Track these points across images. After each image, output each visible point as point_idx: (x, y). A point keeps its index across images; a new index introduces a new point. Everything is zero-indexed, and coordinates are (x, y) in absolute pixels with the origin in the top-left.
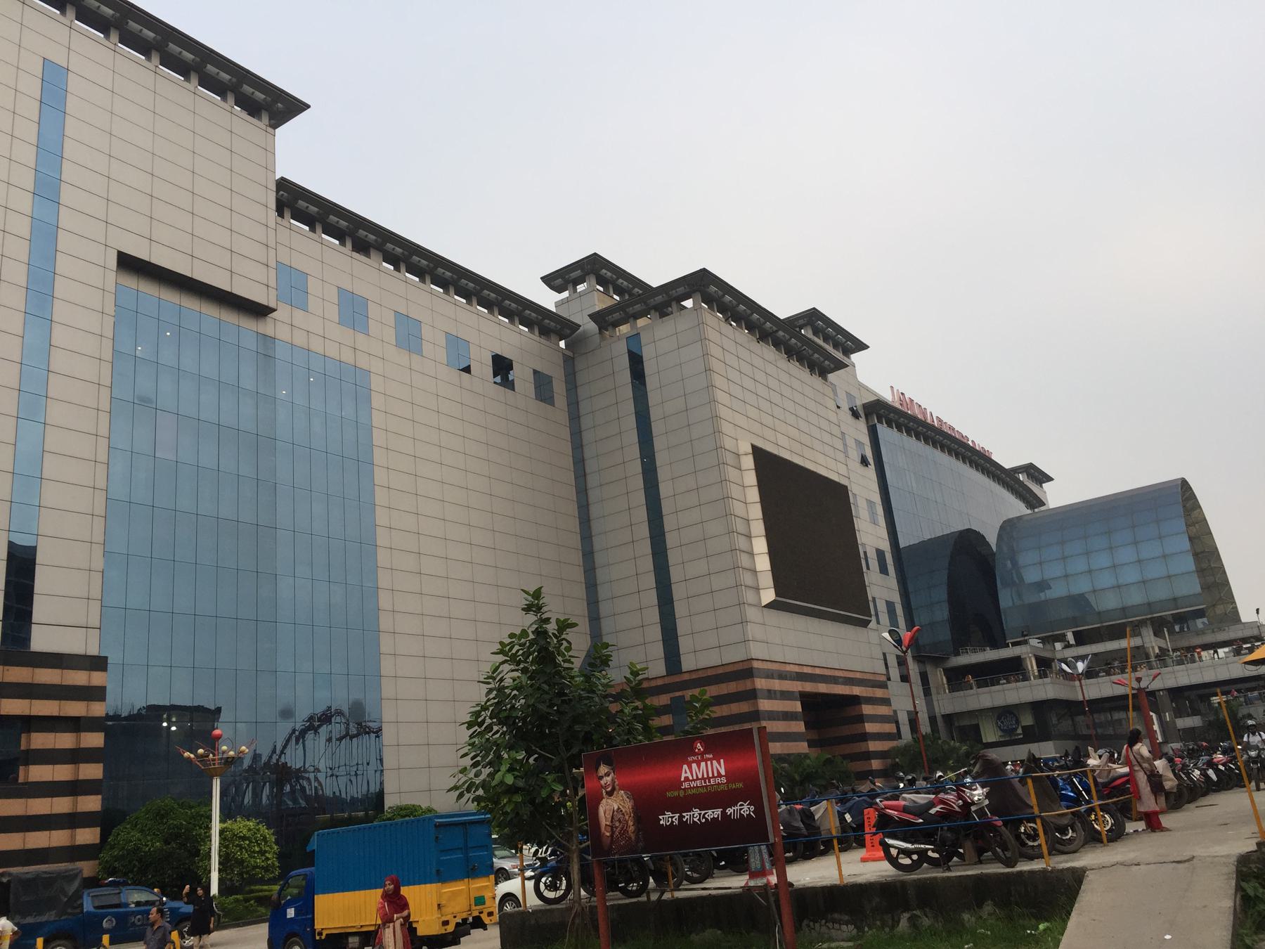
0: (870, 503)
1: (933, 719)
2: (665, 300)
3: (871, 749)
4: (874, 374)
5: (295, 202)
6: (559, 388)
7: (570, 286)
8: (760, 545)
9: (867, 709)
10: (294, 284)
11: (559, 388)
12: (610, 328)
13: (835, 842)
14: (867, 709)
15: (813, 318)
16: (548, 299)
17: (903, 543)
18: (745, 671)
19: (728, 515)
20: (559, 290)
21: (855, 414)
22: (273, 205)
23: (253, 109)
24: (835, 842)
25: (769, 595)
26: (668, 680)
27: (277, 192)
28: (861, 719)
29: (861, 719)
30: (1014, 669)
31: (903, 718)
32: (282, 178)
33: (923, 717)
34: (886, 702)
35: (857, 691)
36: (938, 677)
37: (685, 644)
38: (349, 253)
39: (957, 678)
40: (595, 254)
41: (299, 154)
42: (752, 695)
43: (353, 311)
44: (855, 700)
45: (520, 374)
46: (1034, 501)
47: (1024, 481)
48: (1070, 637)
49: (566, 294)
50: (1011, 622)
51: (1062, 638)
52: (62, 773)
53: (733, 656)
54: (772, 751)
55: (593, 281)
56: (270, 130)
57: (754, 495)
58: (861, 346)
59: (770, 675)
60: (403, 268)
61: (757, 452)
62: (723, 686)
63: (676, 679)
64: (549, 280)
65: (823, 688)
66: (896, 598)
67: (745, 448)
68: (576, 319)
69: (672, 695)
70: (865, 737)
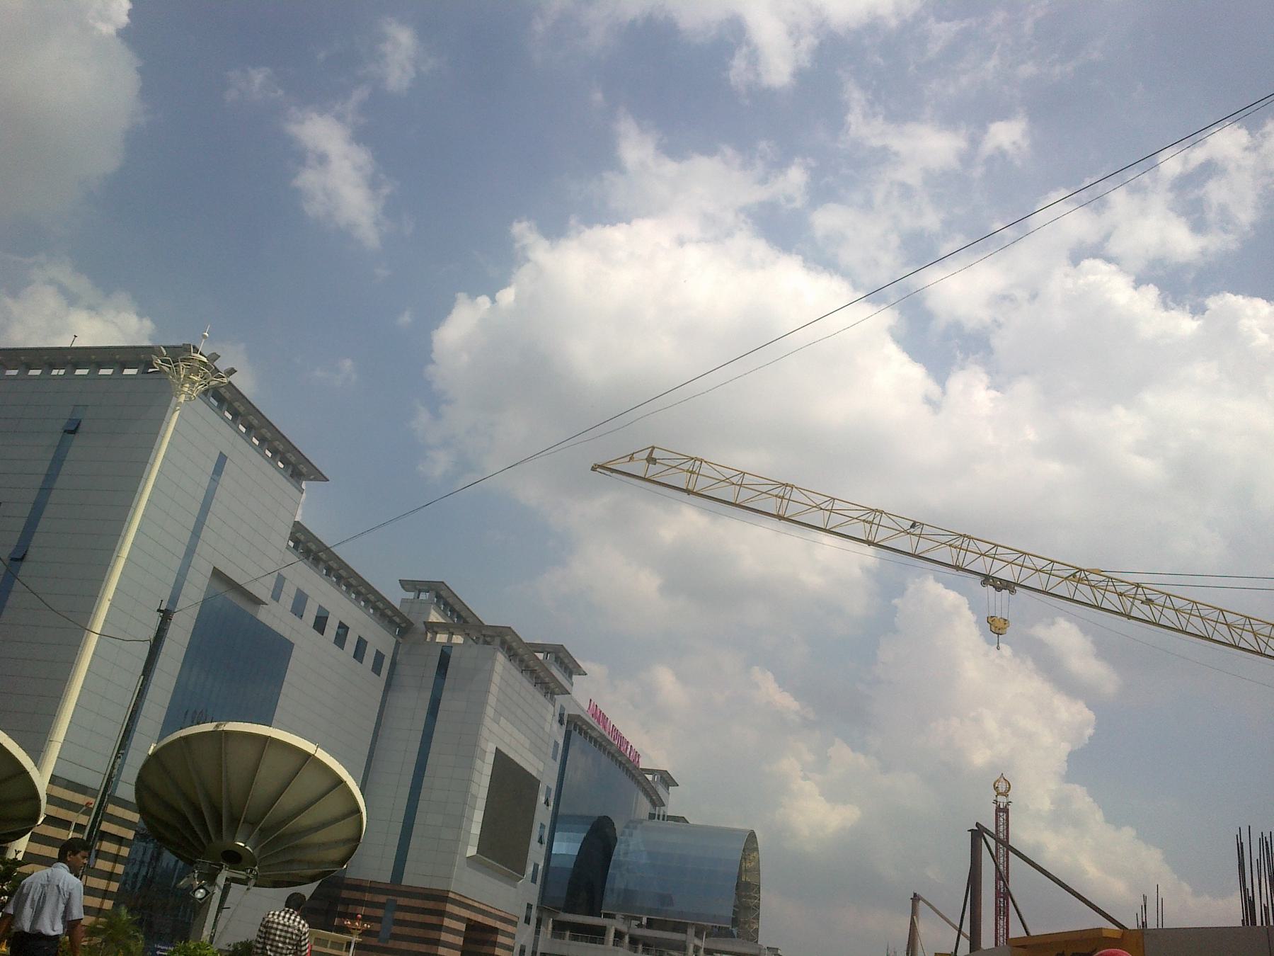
4: (584, 693)
8: (478, 816)
16: (396, 596)
18: (443, 897)
19: (467, 791)
21: (561, 722)
25: (472, 851)
28: (494, 944)
34: (512, 936)
35: (498, 925)
37: (409, 866)
39: (559, 928)
42: (442, 914)
44: (495, 931)
46: (657, 802)
48: (644, 921)
49: (411, 595)
50: (609, 900)
51: (640, 919)
53: (437, 885)
54: (102, 828)
55: (433, 594)
57: (486, 781)
59: (455, 902)
60: (225, 407)
61: (498, 752)
64: (405, 584)
65: (480, 918)
67: (490, 749)
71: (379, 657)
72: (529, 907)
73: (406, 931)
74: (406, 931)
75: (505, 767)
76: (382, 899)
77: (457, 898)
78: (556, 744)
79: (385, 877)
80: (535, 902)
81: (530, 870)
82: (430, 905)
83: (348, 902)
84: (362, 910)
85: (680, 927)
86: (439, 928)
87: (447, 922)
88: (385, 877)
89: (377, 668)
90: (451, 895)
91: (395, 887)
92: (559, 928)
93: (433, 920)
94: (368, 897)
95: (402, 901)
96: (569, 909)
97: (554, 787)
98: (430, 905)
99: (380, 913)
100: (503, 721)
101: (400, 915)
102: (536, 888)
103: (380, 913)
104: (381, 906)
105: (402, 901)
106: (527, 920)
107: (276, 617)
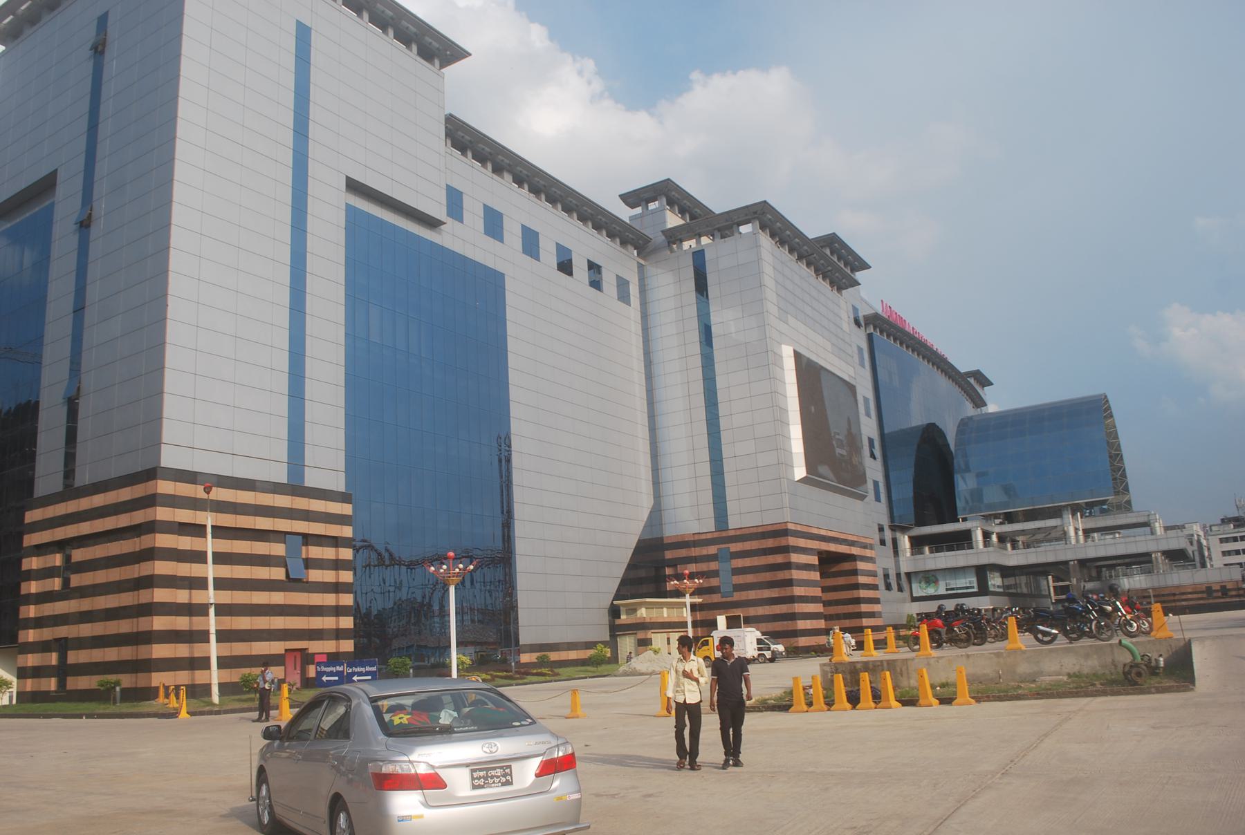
0: (866, 400)
1: (898, 575)
2: (725, 225)
3: (795, 577)
5: (464, 139)
6: (634, 290)
8: (796, 433)
9: (861, 565)
10: (455, 200)
11: (634, 290)
13: (212, 611)
14: (861, 565)
15: (832, 241)
16: (625, 213)
17: (886, 431)
20: (632, 207)
21: (857, 323)
23: (427, 54)
24: (212, 611)
25: (800, 472)
26: (716, 535)
29: (855, 572)
30: (962, 540)
31: (880, 573)
33: (892, 574)
35: (855, 551)
36: (905, 542)
37: (731, 507)
38: (490, 174)
40: (668, 181)
42: (788, 566)
43: (494, 224)
44: (851, 558)
47: (972, 384)
49: (639, 210)
50: (960, 504)
52: (328, 576)
55: (664, 200)
58: (865, 266)
63: (724, 534)
65: (833, 547)
66: (880, 478)
68: (647, 232)
70: (855, 572)
71: (622, 284)
72: (881, 529)
73: (750, 578)
74: (750, 578)
75: (809, 373)
76: (712, 550)
77: (799, 528)
78: (860, 350)
79: (707, 525)
80: (885, 522)
81: (870, 485)
82: (770, 543)
83: (674, 563)
84: (692, 568)
85: (1056, 513)
86: (789, 583)
87: (795, 558)
88: (707, 525)
89: (624, 297)
90: (791, 526)
91: (723, 535)
92: (917, 543)
93: (779, 559)
94: (695, 552)
95: (734, 547)
96: (920, 522)
97: (870, 395)
98: (770, 543)
99: (713, 566)
100: (791, 320)
101: (739, 563)
102: (883, 506)
103: (713, 566)
104: (713, 558)
105: (734, 547)
106: (883, 542)
107: (463, 238)
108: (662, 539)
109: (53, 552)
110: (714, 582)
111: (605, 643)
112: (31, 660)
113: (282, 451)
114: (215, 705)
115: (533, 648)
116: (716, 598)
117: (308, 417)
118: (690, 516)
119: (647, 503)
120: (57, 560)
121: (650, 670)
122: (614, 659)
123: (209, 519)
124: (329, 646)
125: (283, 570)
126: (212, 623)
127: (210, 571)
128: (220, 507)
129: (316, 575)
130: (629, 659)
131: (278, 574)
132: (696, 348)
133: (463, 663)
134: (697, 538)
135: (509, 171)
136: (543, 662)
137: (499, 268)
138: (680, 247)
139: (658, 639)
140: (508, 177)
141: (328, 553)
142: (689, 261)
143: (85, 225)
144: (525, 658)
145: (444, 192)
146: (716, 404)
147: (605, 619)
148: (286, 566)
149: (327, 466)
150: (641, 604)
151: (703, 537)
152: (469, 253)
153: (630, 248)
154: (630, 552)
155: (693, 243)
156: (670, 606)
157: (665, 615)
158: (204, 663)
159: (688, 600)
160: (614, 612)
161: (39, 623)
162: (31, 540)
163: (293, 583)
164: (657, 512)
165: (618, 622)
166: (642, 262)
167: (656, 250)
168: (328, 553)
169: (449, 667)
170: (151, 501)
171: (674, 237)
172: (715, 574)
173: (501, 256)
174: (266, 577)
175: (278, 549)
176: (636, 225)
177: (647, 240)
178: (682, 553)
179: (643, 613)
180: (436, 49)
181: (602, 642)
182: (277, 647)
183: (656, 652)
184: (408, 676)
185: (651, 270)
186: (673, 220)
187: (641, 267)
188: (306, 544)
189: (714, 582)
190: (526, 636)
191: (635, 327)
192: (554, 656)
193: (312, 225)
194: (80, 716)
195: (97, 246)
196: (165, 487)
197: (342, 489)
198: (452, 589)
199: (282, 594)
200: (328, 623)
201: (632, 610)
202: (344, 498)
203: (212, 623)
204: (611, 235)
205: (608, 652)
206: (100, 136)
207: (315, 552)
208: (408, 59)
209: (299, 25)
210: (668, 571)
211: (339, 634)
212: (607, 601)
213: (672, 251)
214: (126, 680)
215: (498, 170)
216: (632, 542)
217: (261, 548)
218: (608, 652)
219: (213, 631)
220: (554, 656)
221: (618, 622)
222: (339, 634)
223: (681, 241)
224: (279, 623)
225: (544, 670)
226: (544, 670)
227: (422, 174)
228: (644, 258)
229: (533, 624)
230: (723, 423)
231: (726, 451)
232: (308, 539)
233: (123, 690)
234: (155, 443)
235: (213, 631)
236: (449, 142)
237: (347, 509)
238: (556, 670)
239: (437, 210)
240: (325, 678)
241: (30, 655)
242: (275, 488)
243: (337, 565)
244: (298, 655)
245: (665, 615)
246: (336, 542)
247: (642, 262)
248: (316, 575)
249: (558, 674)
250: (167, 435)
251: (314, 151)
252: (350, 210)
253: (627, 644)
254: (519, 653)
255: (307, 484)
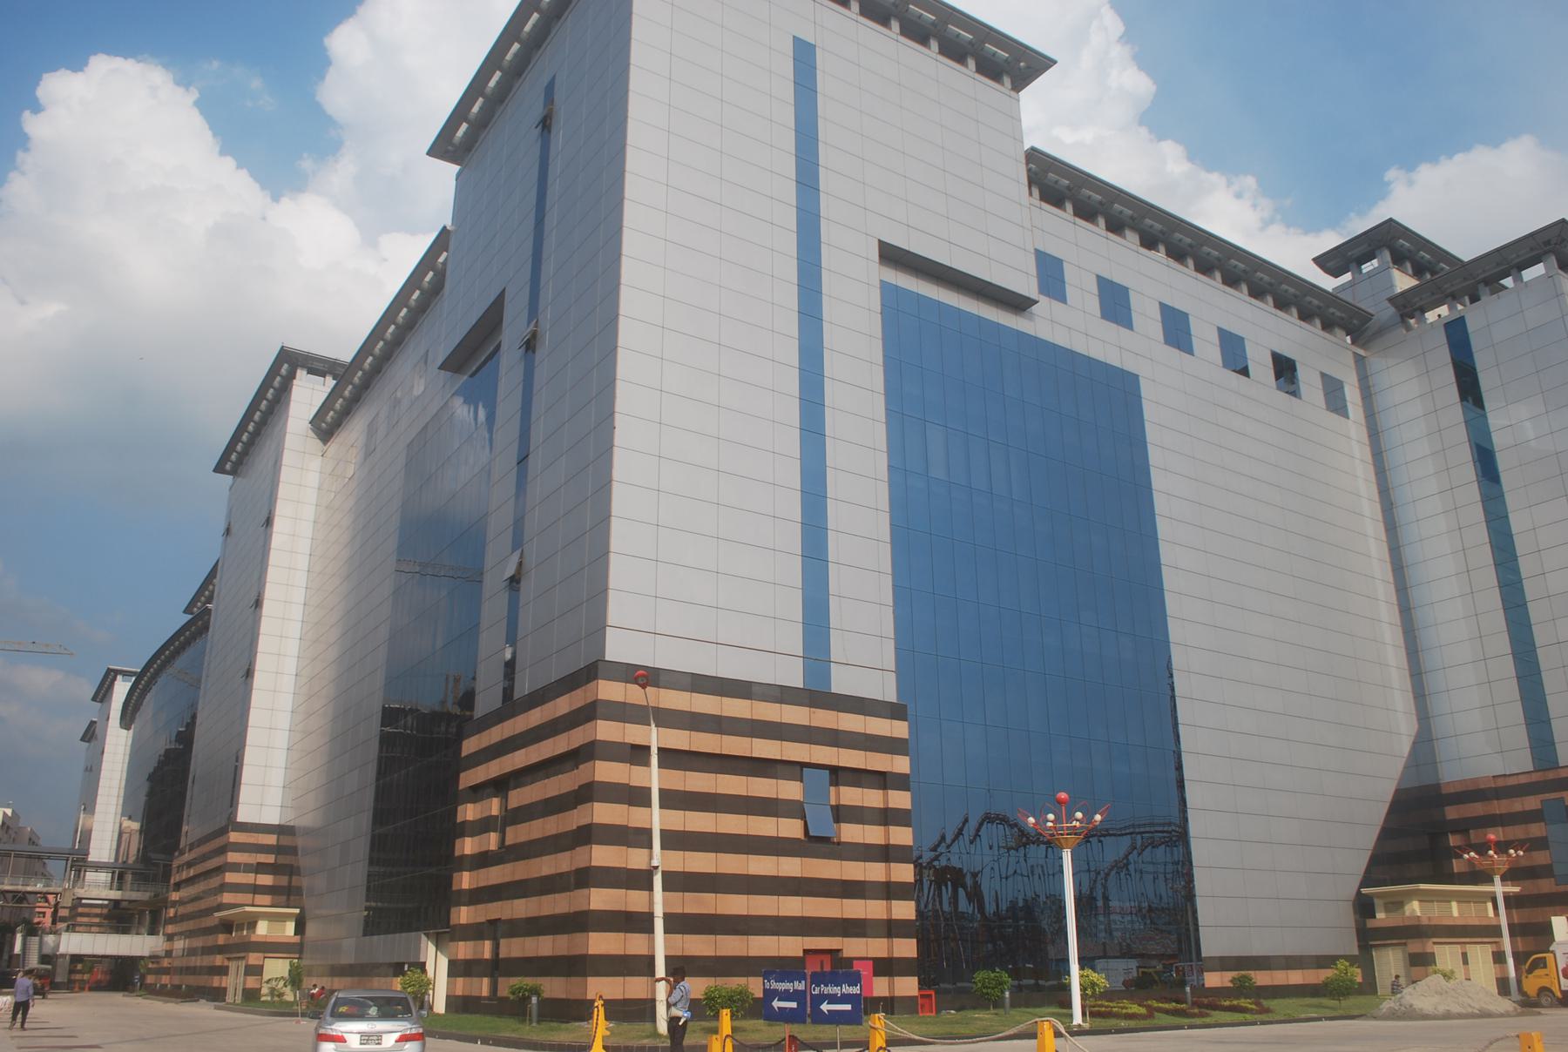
5: (1056, 183)
6: (1352, 394)
7: (1353, 266)
10: (1051, 273)
11: (1352, 394)
12: (1417, 313)
20: (1336, 274)
22: (1026, 182)
23: (991, 70)
24: (658, 880)
26: (1535, 777)
27: (1027, 164)
32: (1033, 149)
38: (1104, 233)
40: (1391, 220)
41: (1050, 118)
43: (1115, 302)
45: (1308, 378)
49: (1348, 277)
52: (872, 834)
55: (1387, 255)
56: (1013, 94)
62: (536, 835)
63: (1551, 775)
69: (1542, 797)
76: (1532, 803)
83: (1462, 827)
88: (1515, 760)
99: (1536, 830)
103: (1536, 830)
108: (1438, 786)
109: (489, 796)
110: (1541, 858)
111: (1352, 960)
112: (464, 950)
113: (794, 640)
114: (660, 1036)
115: (1224, 964)
116: (1546, 886)
117: (833, 587)
118: (1485, 745)
119: (1405, 728)
120: (494, 806)
121: (1442, 1009)
122: (1369, 987)
123: (655, 737)
124: (876, 947)
125: (799, 823)
126: (659, 902)
127: (657, 818)
128: (667, 718)
129: (852, 833)
130: (1396, 988)
131: (791, 828)
132: (1472, 493)
133: (1093, 984)
134: (1501, 783)
135: (1133, 228)
136: (1242, 988)
137: (1130, 365)
138: (1422, 320)
139: (1446, 955)
140: (1132, 238)
141: (872, 798)
142: (1441, 338)
143: (530, 345)
144: (1213, 980)
145: (1033, 257)
146: (1523, 605)
147: (1348, 917)
148: (803, 818)
149: (866, 661)
150: (1411, 895)
151: (1512, 782)
152: (1080, 346)
153: (1339, 332)
154: (1383, 809)
155: (1443, 310)
156: (1462, 898)
157: (1455, 913)
158: (644, 965)
159: (1499, 888)
160: (1364, 907)
161: (478, 896)
162: (468, 778)
163: (816, 845)
164: (1425, 741)
165: (1371, 923)
166: (1361, 352)
167: (1381, 331)
168: (872, 798)
169: (1067, 989)
170: (589, 713)
171: (1408, 307)
172: (1540, 844)
173: (1134, 349)
174: (710, 828)
175: (790, 790)
176: (1347, 296)
177: (1366, 317)
178: (1477, 809)
179: (1414, 908)
180: (1010, 64)
181: (1346, 958)
182: (791, 946)
183: (1447, 976)
184: (998, 1004)
185: (1376, 362)
186: (1403, 282)
187: (1359, 361)
188: (835, 782)
189: (1541, 858)
190: (1212, 943)
191: (1359, 449)
192: (1261, 978)
193: (830, 310)
194: (473, 1040)
195: (542, 372)
196: (609, 690)
197: (892, 696)
198: (1067, 856)
199: (797, 860)
200: (873, 909)
201: (1396, 904)
202: (895, 711)
203: (659, 902)
204: (1305, 316)
205: (1357, 975)
206: (547, 228)
207: (851, 796)
208: (964, 79)
209: (797, 41)
210: (1454, 840)
211: (892, 929)
212: (1350, 887)
213: (1409, 328)
214: (554, 987)
215: (1115, 227)
216: (1387, 791)
217: (762, 787)
218: (1357, 975)
219: (659, 911)
220: (1261, 978)
221: (1371, 923)
222: (892, 929)
223: (1423, 310)
224: (792, 906)
225: (1243, 1002)
226: (1243, 1002)
227: (1000, 237)
228: (1363, 346)
229: (1222, 925)
230: (1530, 589)
231: (1540, 636)
232: (838, 775)
233: (543, 1003)
234: (599, 628)
235: (659, 911)
236: (1036, 192)
237: (899, 729)
238: (1266, 1003)
239: (1024, 283)
240: (776, 1004)
241: (461, 943)
242: (783, 695)
243: (887, 817)
244: (827, 959)
245: (1455, 913)
246: (883, 780)
247: (1361, 352)
248: (852, 833)
249: (1268, 1011)
250: (614, 614)
251: (827, 207)
252: (884, 285)
253: (1389, 962)
254: (1201, 971)
255: (836, 688)
